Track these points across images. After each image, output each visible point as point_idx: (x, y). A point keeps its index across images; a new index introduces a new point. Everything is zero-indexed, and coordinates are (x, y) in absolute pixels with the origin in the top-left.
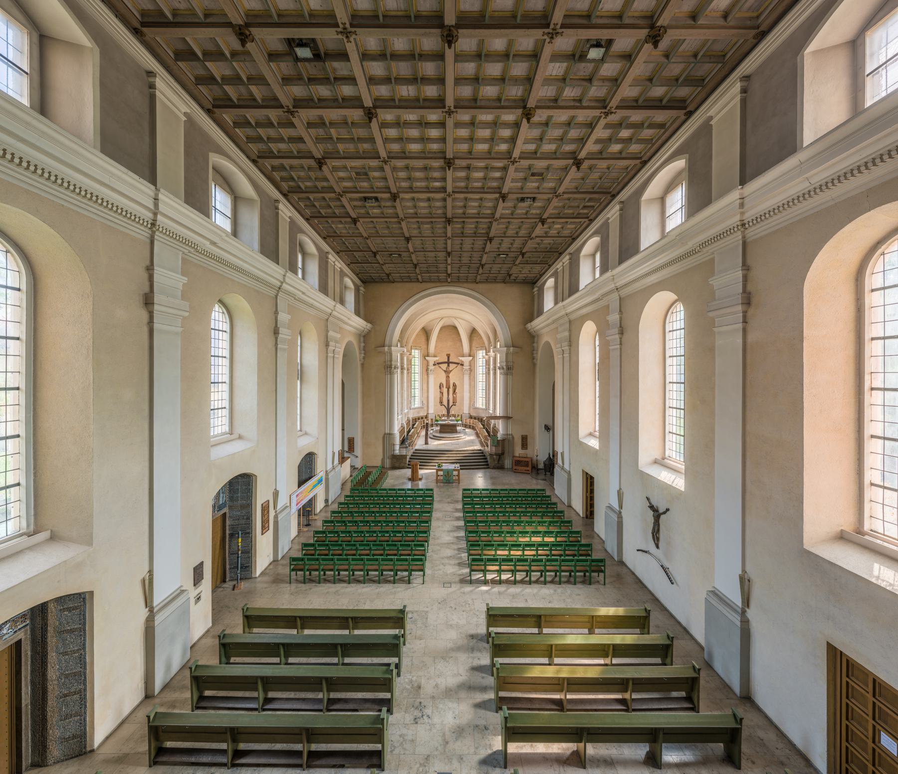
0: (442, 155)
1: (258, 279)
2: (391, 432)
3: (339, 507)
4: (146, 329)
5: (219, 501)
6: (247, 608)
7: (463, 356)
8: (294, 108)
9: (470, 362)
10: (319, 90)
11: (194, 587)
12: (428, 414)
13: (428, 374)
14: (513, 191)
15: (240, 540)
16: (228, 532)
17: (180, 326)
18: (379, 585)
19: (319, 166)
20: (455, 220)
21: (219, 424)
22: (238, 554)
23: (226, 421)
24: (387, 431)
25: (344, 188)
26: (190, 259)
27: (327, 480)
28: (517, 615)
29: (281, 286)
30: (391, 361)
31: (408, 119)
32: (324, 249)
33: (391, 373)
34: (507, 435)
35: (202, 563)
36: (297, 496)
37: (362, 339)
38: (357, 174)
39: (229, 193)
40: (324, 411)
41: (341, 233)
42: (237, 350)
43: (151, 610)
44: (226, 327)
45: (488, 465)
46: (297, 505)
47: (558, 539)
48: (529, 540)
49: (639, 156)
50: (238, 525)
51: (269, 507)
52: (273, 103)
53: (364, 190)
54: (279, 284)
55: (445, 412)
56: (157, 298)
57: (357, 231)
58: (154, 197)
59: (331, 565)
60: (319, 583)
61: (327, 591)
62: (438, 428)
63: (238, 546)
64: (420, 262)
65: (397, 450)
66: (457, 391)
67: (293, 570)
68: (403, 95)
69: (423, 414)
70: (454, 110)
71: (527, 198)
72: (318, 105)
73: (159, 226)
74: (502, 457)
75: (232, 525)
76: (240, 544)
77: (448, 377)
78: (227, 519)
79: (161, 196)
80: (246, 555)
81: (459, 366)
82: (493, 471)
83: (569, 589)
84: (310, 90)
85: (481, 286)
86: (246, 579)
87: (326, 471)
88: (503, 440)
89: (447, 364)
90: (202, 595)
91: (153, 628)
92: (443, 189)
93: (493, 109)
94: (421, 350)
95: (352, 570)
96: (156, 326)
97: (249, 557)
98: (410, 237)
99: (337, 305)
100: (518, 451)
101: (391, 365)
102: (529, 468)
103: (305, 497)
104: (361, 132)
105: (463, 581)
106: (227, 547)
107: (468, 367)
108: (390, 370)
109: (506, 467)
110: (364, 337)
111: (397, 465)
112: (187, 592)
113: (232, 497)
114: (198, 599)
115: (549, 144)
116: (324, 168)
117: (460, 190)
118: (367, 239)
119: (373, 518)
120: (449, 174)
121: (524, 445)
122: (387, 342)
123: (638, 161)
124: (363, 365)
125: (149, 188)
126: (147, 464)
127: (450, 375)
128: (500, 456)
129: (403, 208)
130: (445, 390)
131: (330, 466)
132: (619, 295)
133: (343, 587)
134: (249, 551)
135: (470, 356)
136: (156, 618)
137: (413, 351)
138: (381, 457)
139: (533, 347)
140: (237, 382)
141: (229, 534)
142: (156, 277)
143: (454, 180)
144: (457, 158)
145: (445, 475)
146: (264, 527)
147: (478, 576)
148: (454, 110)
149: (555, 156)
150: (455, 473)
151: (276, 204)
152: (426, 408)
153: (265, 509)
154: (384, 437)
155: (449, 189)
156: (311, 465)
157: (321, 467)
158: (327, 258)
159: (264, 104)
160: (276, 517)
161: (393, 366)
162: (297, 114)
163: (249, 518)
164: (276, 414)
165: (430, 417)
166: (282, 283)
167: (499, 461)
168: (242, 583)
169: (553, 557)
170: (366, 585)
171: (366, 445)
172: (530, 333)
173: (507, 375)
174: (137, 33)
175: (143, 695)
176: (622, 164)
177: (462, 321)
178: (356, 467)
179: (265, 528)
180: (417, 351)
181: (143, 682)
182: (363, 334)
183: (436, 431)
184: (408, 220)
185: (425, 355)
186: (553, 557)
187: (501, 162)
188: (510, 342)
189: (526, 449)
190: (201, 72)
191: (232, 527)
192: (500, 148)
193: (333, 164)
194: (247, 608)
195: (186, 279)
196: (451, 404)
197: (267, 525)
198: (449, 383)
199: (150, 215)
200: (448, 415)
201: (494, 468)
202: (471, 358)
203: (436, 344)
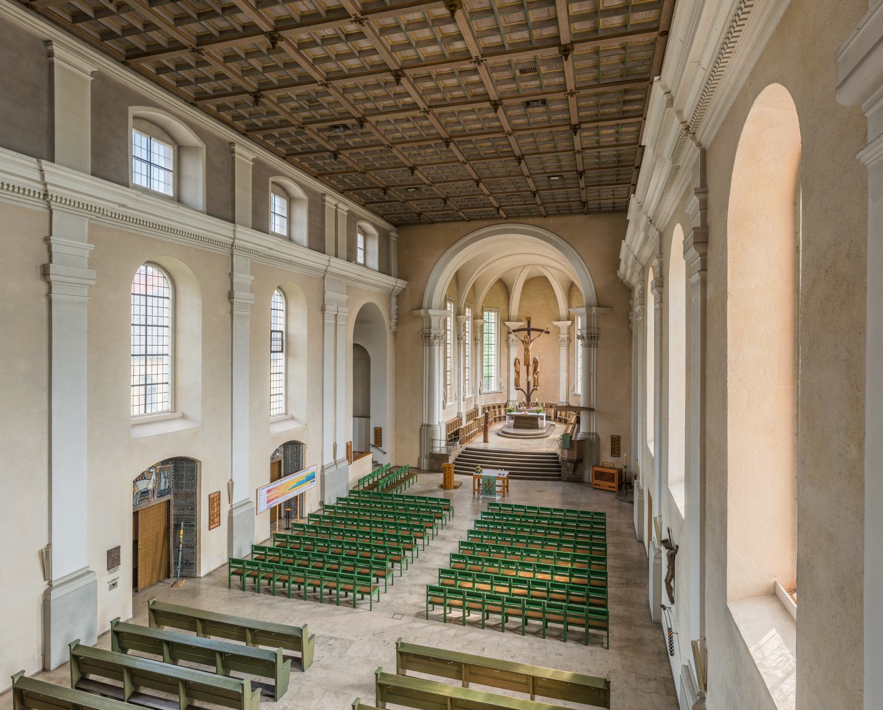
0: (555, 40)
1: (197, 237)
2: (430, 423)
3: (475, 527)
4: (44, 300)
5: (159, 485)
6: (154, 601)
7: (559, 320)
8: (197, 46)
9: (569, 328)
10: (216, 22)
11: (107, 572)
12: (508, 401)
13: (508, 347)
14: (508, 95)
15: (182, 532)
16: (172, 522)
17: (86, 295)
18: (320, 604)
19: (256, 100)
20: (583, 126)
21: (277, 406)
22: (179, 548)
23: (168, 397)
24: (425, 422)
25: (304, 118)
26: (99, 223)
27: (323, 477)
28: (433, 658)
29: (233, 243)
30: (430, 328)
31: (326, 35)
32: (317, 190)
33: (430, 345)
34: (590, 433)
35: (118, 549)
36: (268, 491)
37: (394, 300)
38: (522, 71)
39: (169, 144)
40: (319, 392)
41: (333, 169)
42: (181, 318)
43: (50, 584)
44: (168, 293)
45: (560, 475)
46: (268, 502)
47: (574, 580)
48: (515, 574)
49: (655, 26)
50: (183, 515)
51: (219, 499)
52: (175, 46)
53: (326, 118)
54: (231, 241)
55: (524, 399)
56: (53, 269)
57: (451, 155)
58: (39, 168)
59: (286, 575)
60: (258, 592)
61: (261, 601)
62: (512, 422)
63: (180, 538)
64: (450, 195)
65: (440, 445)
66: (538, 370)
67: (430, 602)
68: (304, 10)
69: (500, 401)
70: (363, 17)
71: (533, 101)
72: (220, 39)
73: (52, 196)
74: (580, 465)
75: (177, 515)
76: (181, 537)
77: (527, 350)
78: (172, 508)
79: (44, 167)
80: (191, 551)
81: (543, 334)
82: (566, 484)
83: (553, 645)
84: (202, 25)
85: (551, 221)
86: (190, 577)
87: (323, 467)
88: (582, 442)
89: (526, 333)
90: (120, 583)
91: (50, 601)
92: (563, 87)
93: (407, 7)
94: (498, 312)
95: (487, 611)
96: (53, 296)
97: (193, 554)
98: (523, 155)
99: (331, 259)
100: (607, 458)
101: (430, 333)
102: (615, 484)
103: (283, 494)
104: (450, 29)
105: (419, 615)
106: (172, 539)
107: (566, 336)
108: (429, 340)
109: (586, 480)
110: (398, 296)
111: (436, 467)
112: (94, 573)
113: (177, 483)
114: (113, 585)
115: (511, 32)
116: (403, 80)
117: (438, 103)
118: (465, 163)
119: (343, 526)
120: (568, 66)
121: (616, 450)
122: (425, 304)
123: (655, 34)
124: (395, 334)
125: (30, 161)
126: (46, 436)
127: (530, 347)
128: (578, 463)
129: (509, 119)
130: (523, 369)
131: (328, 460)
132: (657, 230)
133: (280, 601)
134: (192, 546)
135: (568, 319)
136: (52, 592)
137: (486, 313)
138: (418, 455)
139: (630, 305)
140: (180, 355)
141: (174, 525)
142: (54, 248)
143: (576, 71)
144: (406, 68)
145: (485, 485)
146: (213, 521)
147: (439, 611)
148: (363, 17)
149: (530, 46)
150: (498, 482)
151: (232, 147)
152: (505, 393)
153: (215, 500)
154: (421, 429)
155: (570, 86)
156: (298, 456)
157: (311, 462)
158: (324, 201)
159: (170, 47)
160: (231, 512)
161: (432, 336)
162: (366, 21)
163: (193, 508)
164: (232, 392)
165: (511, 406)
166: (234, 239)
167: (574, 470)
168: (184, 581)
169: (515, 597)
170: (306, 602)
171: (399, 437)
172: (624, 285)
173: (590, 346)
174: (28, 7)
175: (41, 668)
176: (641, 40)
177: (554, 270)
178: (378, 463)
179: (214, 521)
180: (492, 314)
181: (40, 654)
182: (395, 294)
183: (508, 427)
184: (518, 133)
185: (504, 319)
186: (515, 597)
187: (447, 67)
188: (594, 300)
189: (619, 456)
190: (176, 12)
191: (178, 518)
192: (455, 47)
193: (277, 94)
194: (154, 601)
195: (93, 246)
196: (532, 388)
197: (216, 520)
198: (529, 359)
199: (41, 186)
200: (528, 404)
201: (568, 481)
202: (569, 323)
203: (520, 303)
